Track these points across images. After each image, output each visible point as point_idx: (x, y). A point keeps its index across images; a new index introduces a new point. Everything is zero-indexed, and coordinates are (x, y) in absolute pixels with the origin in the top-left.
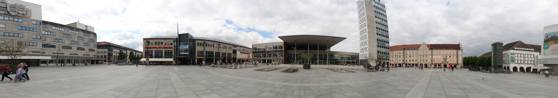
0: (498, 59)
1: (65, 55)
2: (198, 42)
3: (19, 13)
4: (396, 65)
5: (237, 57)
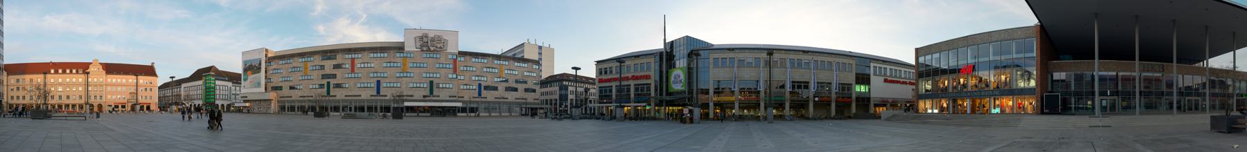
1: (363, 97)
2: (716, 56)
3: (437, 47)
4: (376, 108)
5: (872, 95)
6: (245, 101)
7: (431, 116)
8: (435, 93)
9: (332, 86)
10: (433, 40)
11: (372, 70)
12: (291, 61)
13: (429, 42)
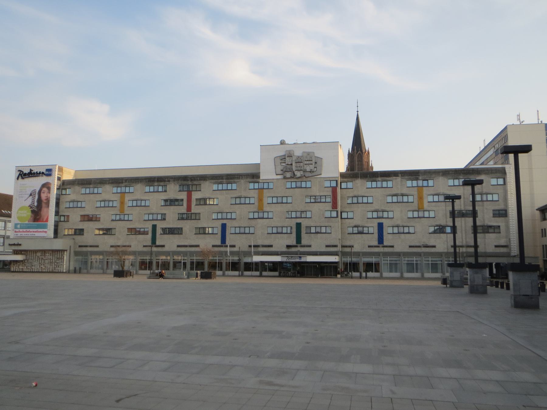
0: (58, 253)
3: (305, 171)
6: (16, 252)
7: (280, 276)
8: (304, 242)
9: (159, 231)
10: (299, 161)
11: (216, 209)
12: (100, 190)
13: (294, 164)
